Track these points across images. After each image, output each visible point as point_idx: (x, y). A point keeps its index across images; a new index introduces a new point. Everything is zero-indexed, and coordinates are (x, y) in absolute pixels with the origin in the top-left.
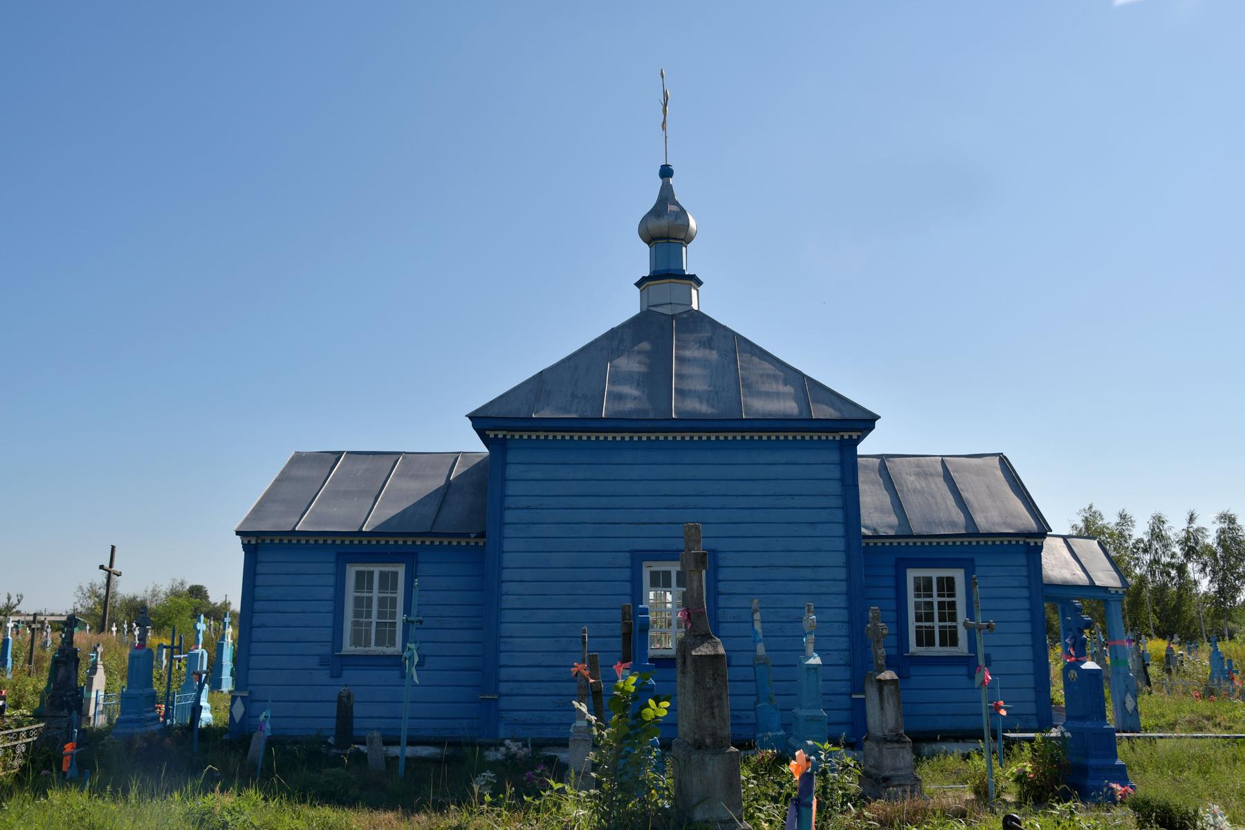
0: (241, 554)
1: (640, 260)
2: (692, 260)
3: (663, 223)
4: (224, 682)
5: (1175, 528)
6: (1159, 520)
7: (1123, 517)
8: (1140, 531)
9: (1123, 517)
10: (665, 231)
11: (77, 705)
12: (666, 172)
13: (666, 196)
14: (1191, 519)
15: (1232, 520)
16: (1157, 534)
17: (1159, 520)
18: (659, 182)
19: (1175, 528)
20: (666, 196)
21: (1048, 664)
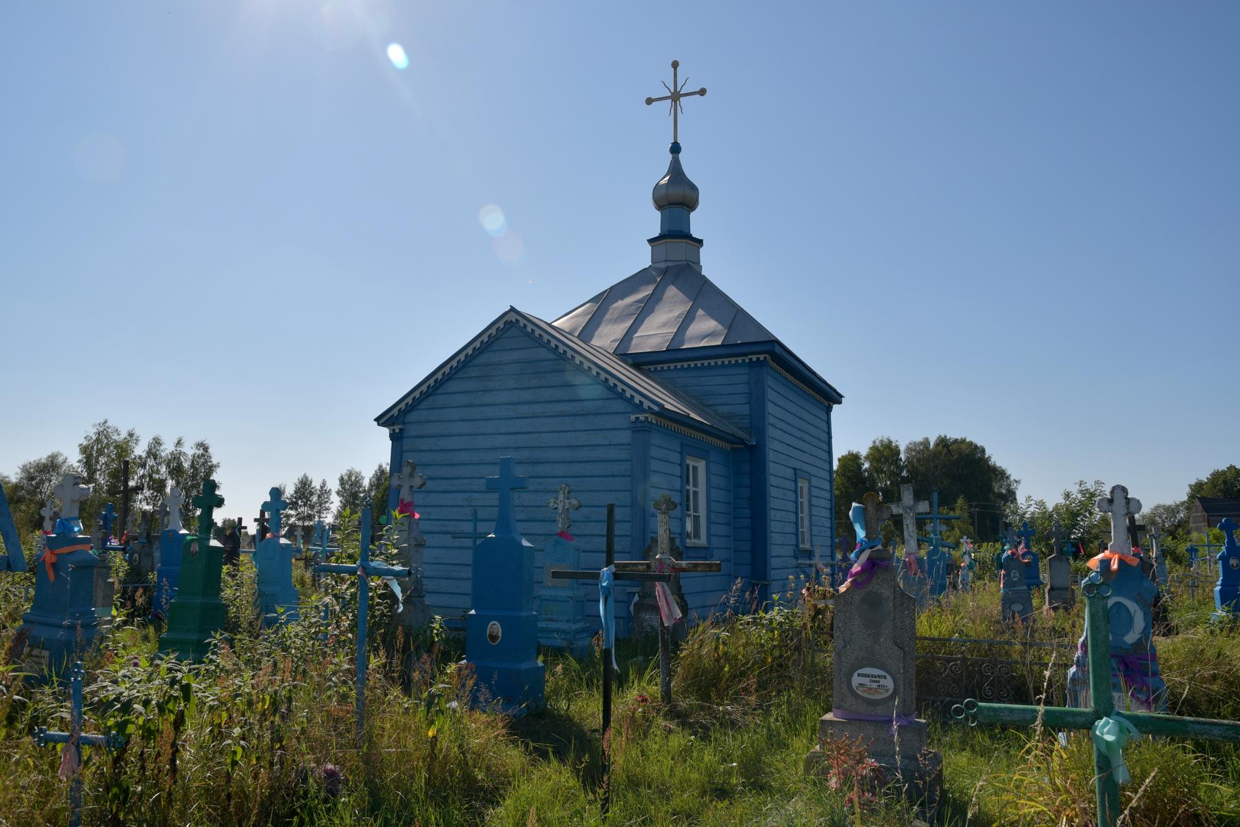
0: (388, 444)
1: (653, 223)
2: (698, 224)
3: (678, 192)
4: (1136, 620)
5: (167, 449)
6: (157, 442)
7: (131, 435)
8: (140, 450)
9: (131, 435)
10: (677, 199)
11: (129, 545)
12: (675, 149)
13: (676, 171)
14: (179, 443)
15: (206, 449)
16: (152, 453)
17: (157, 442)
18: (669, 157)
19: (167, 449)
20: (676, 171)
21: (218, 579)
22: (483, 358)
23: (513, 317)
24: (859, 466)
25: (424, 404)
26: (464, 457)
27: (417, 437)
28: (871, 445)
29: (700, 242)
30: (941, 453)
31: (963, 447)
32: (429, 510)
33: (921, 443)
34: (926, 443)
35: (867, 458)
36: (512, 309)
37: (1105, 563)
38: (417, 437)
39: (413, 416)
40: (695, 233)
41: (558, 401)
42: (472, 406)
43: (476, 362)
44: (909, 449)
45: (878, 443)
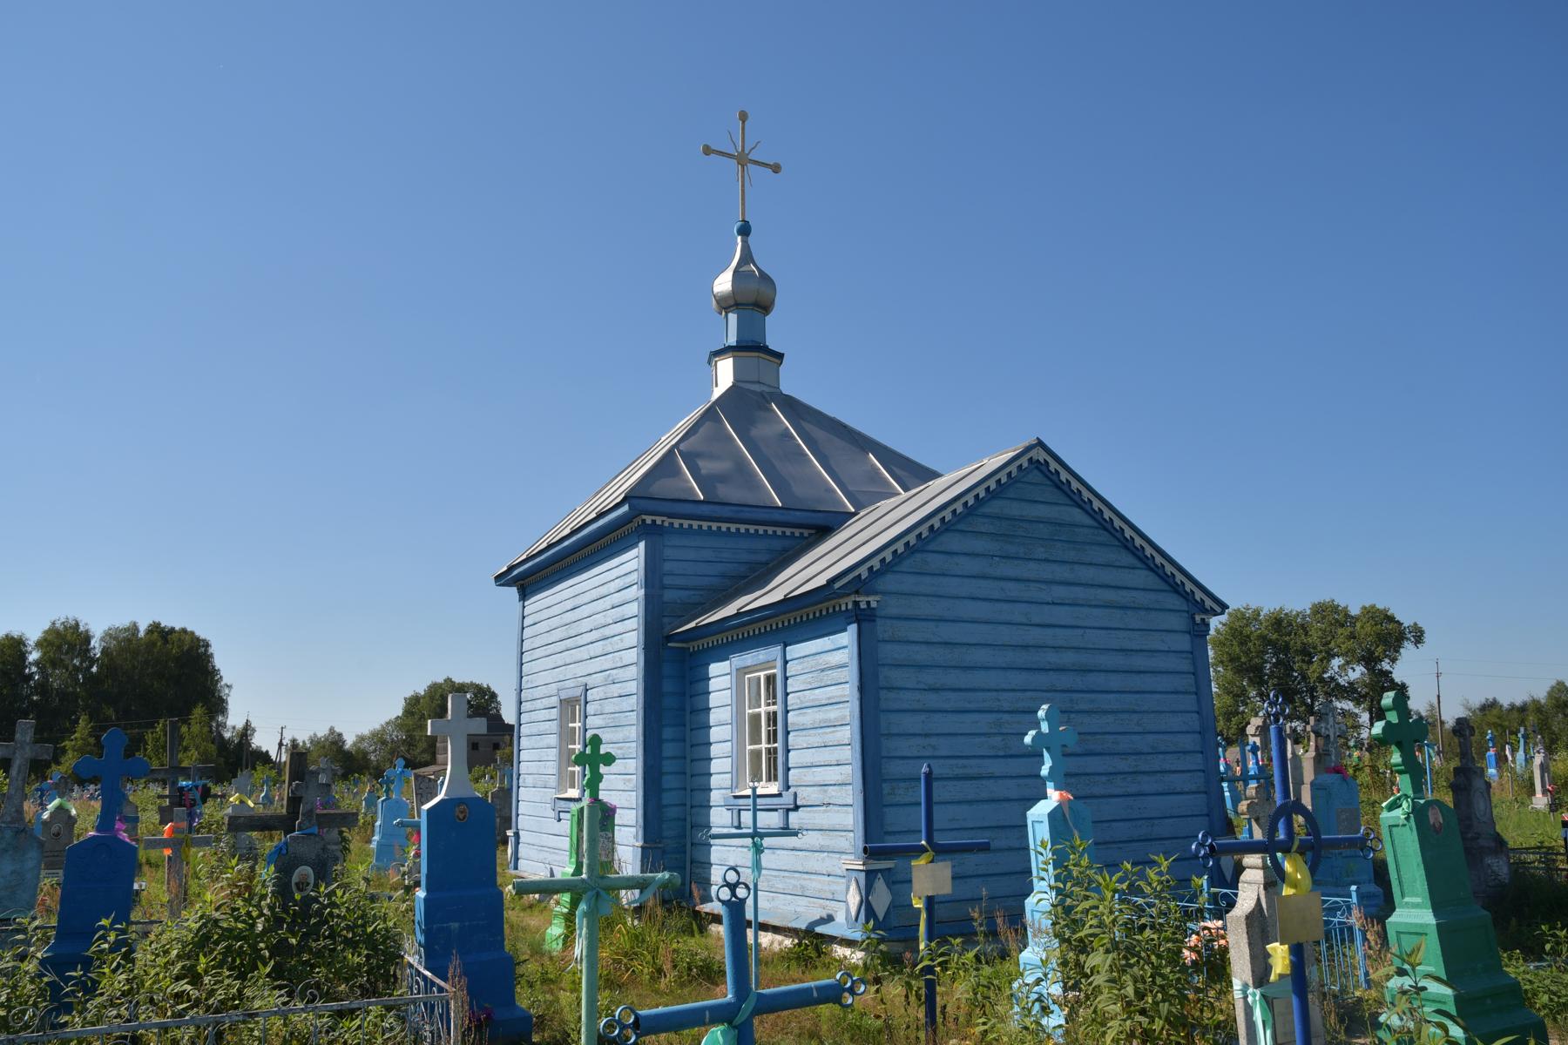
22: (995, 507)
23: (1041, 456)
24: (23, 656)
25: (906, 565)
26: (981, 656)
27: (898, 618)
28: (47, 626)
29: (780, 356)
30: (154, 644)
31: (188, 638)
32: (933, 741)
33: (126, 630)
34: (134, 628)
35: (39, 644)
36: (1040, 444)
37: (426, 789)
38: (898, 618)
39: (889, 582)
40: (772, 343)
41: (1017, 580)
42: (984, 577)
43: (986, 510)
44: (109, 635)
45: (58, 625)
